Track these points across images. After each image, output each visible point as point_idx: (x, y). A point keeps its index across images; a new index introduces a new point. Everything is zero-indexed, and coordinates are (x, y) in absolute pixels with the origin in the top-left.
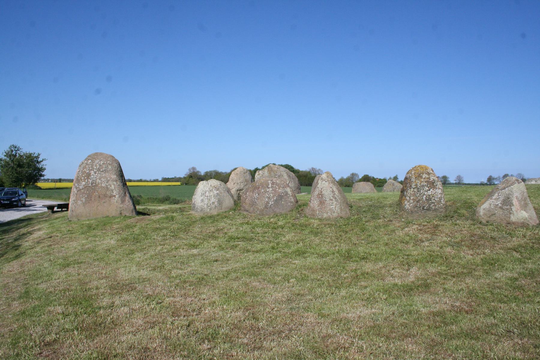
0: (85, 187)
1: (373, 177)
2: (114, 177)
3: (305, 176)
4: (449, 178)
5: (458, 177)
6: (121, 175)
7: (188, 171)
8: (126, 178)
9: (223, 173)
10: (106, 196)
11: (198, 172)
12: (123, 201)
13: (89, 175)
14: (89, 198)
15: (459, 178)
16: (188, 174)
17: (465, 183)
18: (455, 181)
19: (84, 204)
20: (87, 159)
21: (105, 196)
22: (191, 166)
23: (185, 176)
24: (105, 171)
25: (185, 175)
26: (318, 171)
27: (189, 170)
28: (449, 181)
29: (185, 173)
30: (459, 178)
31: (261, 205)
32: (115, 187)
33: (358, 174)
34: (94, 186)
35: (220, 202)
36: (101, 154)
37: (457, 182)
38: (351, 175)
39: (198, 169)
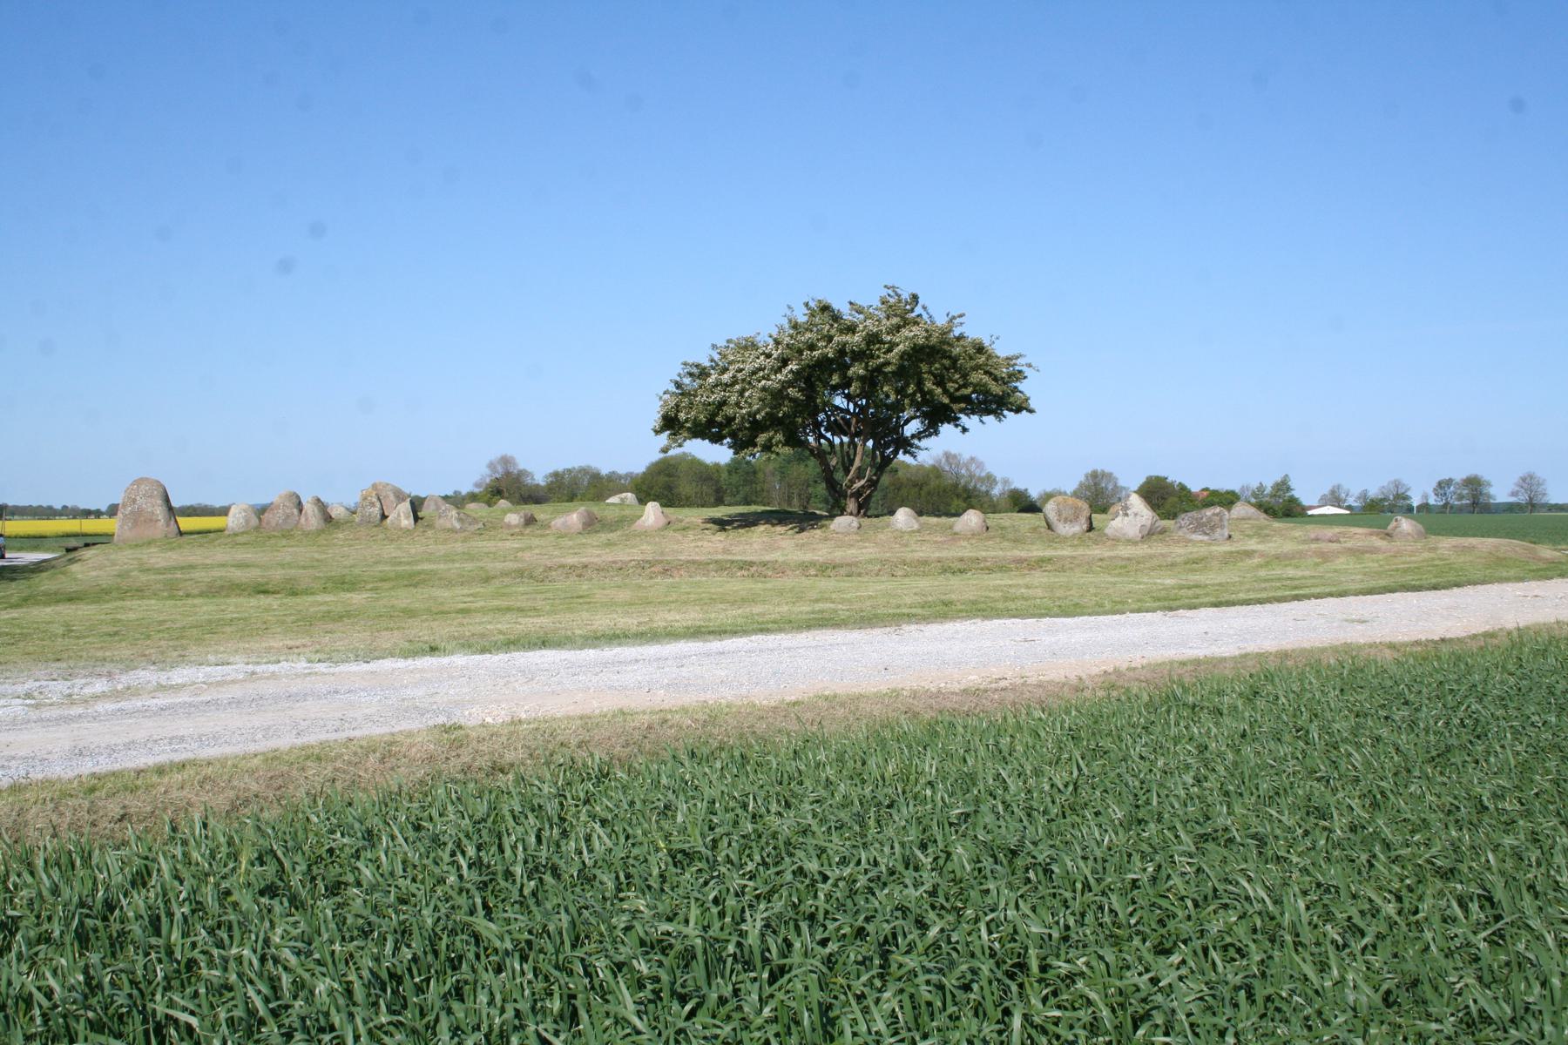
0: (132, 512)
1: (1183, 488)
2: (159, 502)
3: (915, 485)
4: (1489, 485)
5: (1524, 480)
6: (167, 500)
7: (487, 471)
8: (175, 503)
9: (620, 477)
10: (152, 520)
11: (522, 473)
12: (168, 525)
13: (134, 501)
14: (135, 523)
15: (1528, 482)
16: (488, 480)
17: (1553, 501)
18: (1514, 494)
19: (130, 529)
20: (132, 484)
21: (151, 520)
22: (495, 455)
23: (477, 490)
24: (151, 496)
25: (477, 485)
26: (967, 465)
27: (491, 466)
28: (1489, 496)
29: (476, 478)
30: (1528, 482)
31: (273, 524)
32: (160, 511)
33: (1116, 474)
34: (140, 512)
35: (247, 522)
36: (147, 479)
37: (1522, 498)
38: (280, 497)
39: (522, 464)
